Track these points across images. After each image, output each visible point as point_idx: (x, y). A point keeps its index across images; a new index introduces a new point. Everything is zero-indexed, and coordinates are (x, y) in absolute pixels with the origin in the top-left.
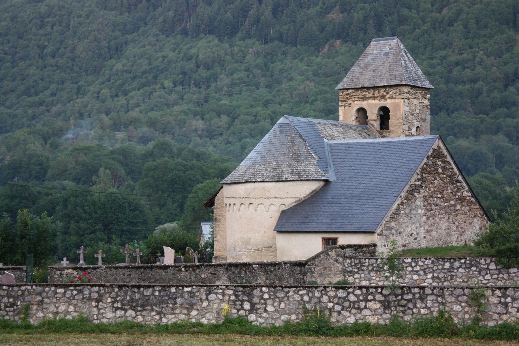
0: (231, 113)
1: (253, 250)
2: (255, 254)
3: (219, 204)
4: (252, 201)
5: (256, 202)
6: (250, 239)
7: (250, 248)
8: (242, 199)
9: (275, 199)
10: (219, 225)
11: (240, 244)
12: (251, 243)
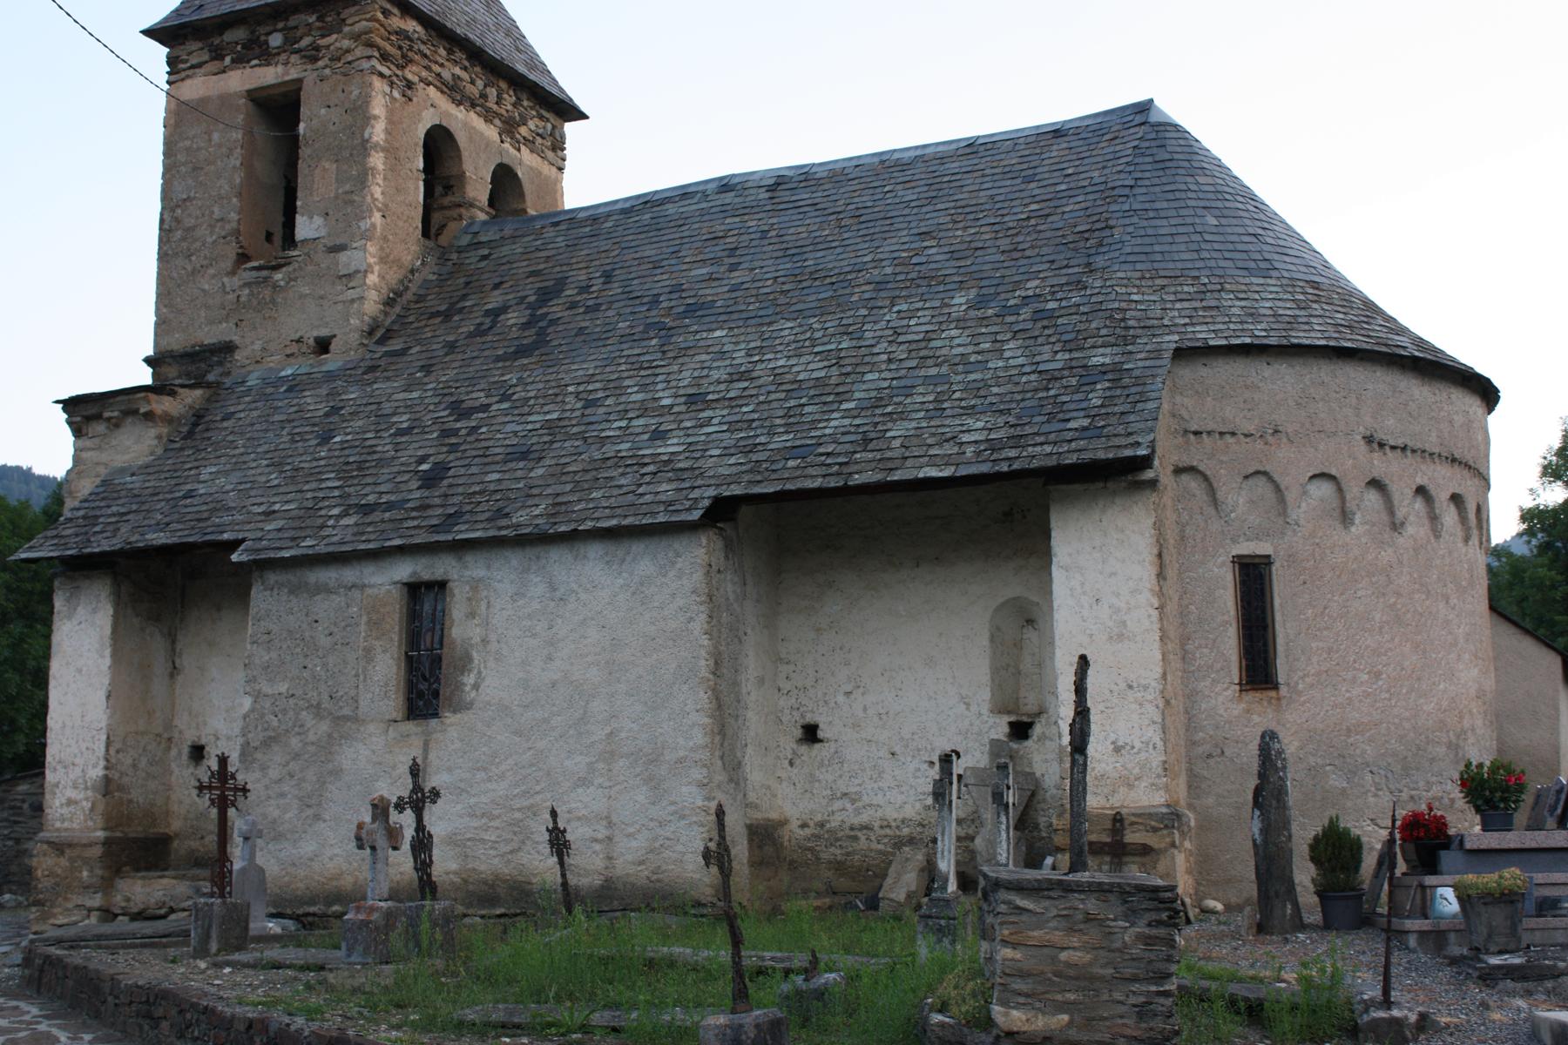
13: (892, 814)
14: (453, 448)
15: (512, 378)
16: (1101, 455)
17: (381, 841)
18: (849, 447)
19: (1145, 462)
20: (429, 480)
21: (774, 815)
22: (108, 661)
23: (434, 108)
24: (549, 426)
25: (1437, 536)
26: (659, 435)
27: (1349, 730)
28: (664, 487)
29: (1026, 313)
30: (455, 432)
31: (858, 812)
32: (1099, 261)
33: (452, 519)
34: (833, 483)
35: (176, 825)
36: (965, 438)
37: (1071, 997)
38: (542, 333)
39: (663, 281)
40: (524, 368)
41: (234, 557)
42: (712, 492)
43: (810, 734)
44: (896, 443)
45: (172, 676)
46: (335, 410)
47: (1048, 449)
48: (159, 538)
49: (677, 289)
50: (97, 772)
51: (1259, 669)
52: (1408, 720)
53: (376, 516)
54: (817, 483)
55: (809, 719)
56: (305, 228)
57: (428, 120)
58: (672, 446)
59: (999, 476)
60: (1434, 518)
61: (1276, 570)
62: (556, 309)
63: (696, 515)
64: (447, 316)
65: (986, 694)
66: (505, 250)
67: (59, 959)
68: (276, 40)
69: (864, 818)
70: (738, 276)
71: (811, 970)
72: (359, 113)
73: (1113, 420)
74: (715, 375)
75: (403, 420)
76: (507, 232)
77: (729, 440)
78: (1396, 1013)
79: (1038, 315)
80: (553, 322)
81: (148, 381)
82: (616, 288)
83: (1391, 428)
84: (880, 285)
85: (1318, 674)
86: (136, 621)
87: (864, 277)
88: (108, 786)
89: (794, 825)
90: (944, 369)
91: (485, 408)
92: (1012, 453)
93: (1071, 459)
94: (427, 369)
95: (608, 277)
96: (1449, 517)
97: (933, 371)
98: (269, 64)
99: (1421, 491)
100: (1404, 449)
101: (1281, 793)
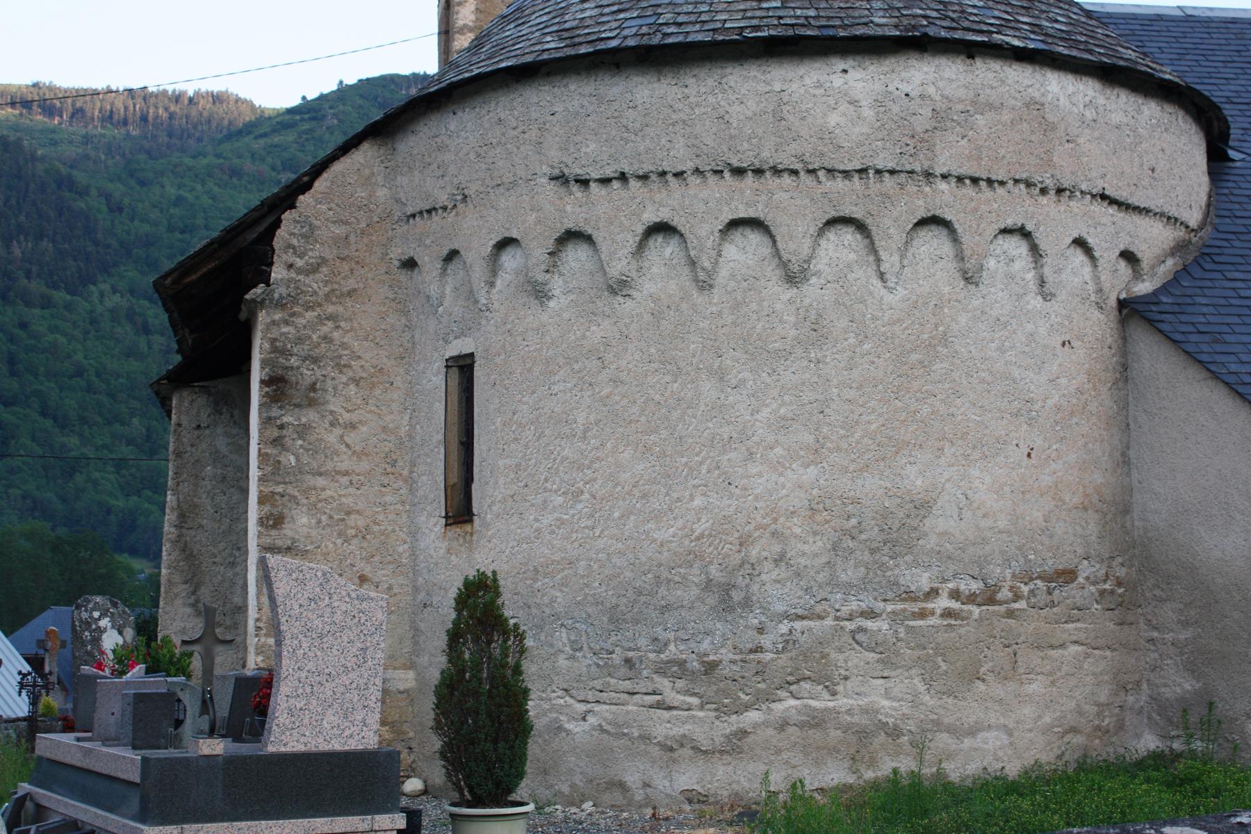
0: (925, 813)
1: (944, 602)
2: (966, 630)
3: (313, 269)
4: (944, 198)
5: (976, 213)
6: (923, 507)
7: (924, 581)
8: (840, 184)
9: (1099, 208)
10: (303, 431)
11: (810, 549)
12: (931, 542)
27: (536, 570)
51: (460, 511)
52: (621, 553)
83: (593, 155)
85: (504, 500)
99: (1080, 243)
100: (862, 171)
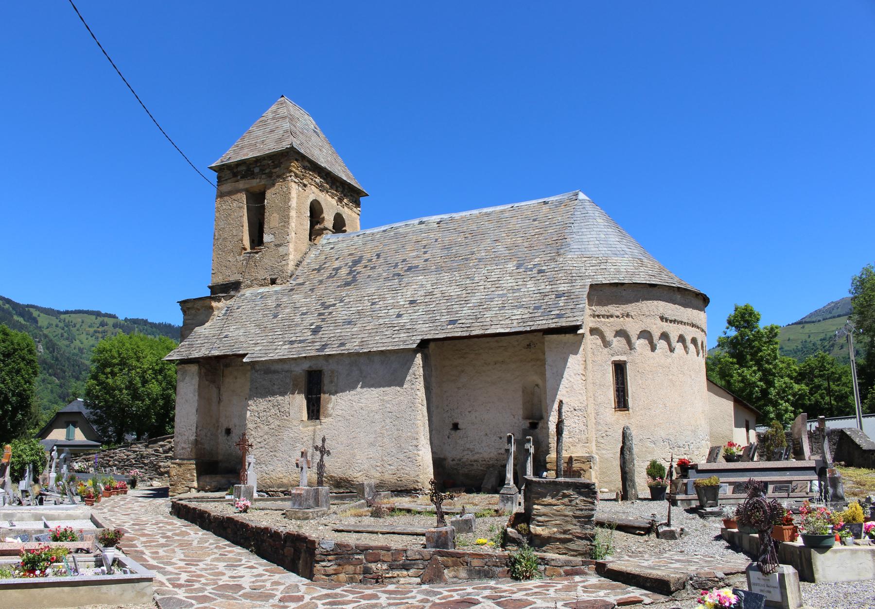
13: (486, 456)
14: (323, 320)
15: (344, 294)
16: (564, 324)
17: (305, 466)
18: (471, 321)
19: (578, 327)
20: (315, 331)
21: (442, 456)
22: (197, 397)
23: (313, 193)
24: (359, 312)
25: (687, 353)
26: (399, 316)
28: (402, 335)
29: (535, 271)
30: (323, 314)
31: (473, 455)
32: (562, 251)
33: (324, 347)
34: (465, 334)
35: (220, 458)
36: (514, 317)
37: (558, 522)
38: (354, 276)
39: (399, 257)
40: (348, 290)
41: (244, 360)
42: (420, 337)
43: (456, 427)
44: (488, 319)
45: (219, 403)
46: (278, 305)
47: (544, 322)
48: (216, 353)
49: (404, 260)
50: (193, 438)
51: (622, 402)
53: (295, 345)
54: (459, 334)
55: (456, 421)
56: (267, 238)
57: (312, 198)
58: (404, 320)
59: (526, 332)
60: (685, 347)
61: (628, 366)
62: (359, 268)
63: (415, 346)
64: (319, 270)
65: (521, 412)
66: (340, 245)
67: (186, 506)
68: (257, 170)
69: (476, 457)
70: (427, 256)
71: (462, 513)
72: (286, 197)
73: (568, 311)
74: (420, 293)
75: (304, 309)
76: (340, 239)
77: (426, 317)
78: (672, 528)
79: (540, 272)
80: (358, 273)
81: (209, 295)
82: (381, 260)
84: (480, 260)
86: (207, 383)
87: (474, 257)
88: (196, 442)
89: (450, 460)
90: (505, 292)
91: (334, 305)
92: (531, 323)
93: (553, 326)
94: (312, 290)
95: (378, 256)
96: (692, 347)
97: (501, 292)
98: (254, 178)
101: (630, 450)
